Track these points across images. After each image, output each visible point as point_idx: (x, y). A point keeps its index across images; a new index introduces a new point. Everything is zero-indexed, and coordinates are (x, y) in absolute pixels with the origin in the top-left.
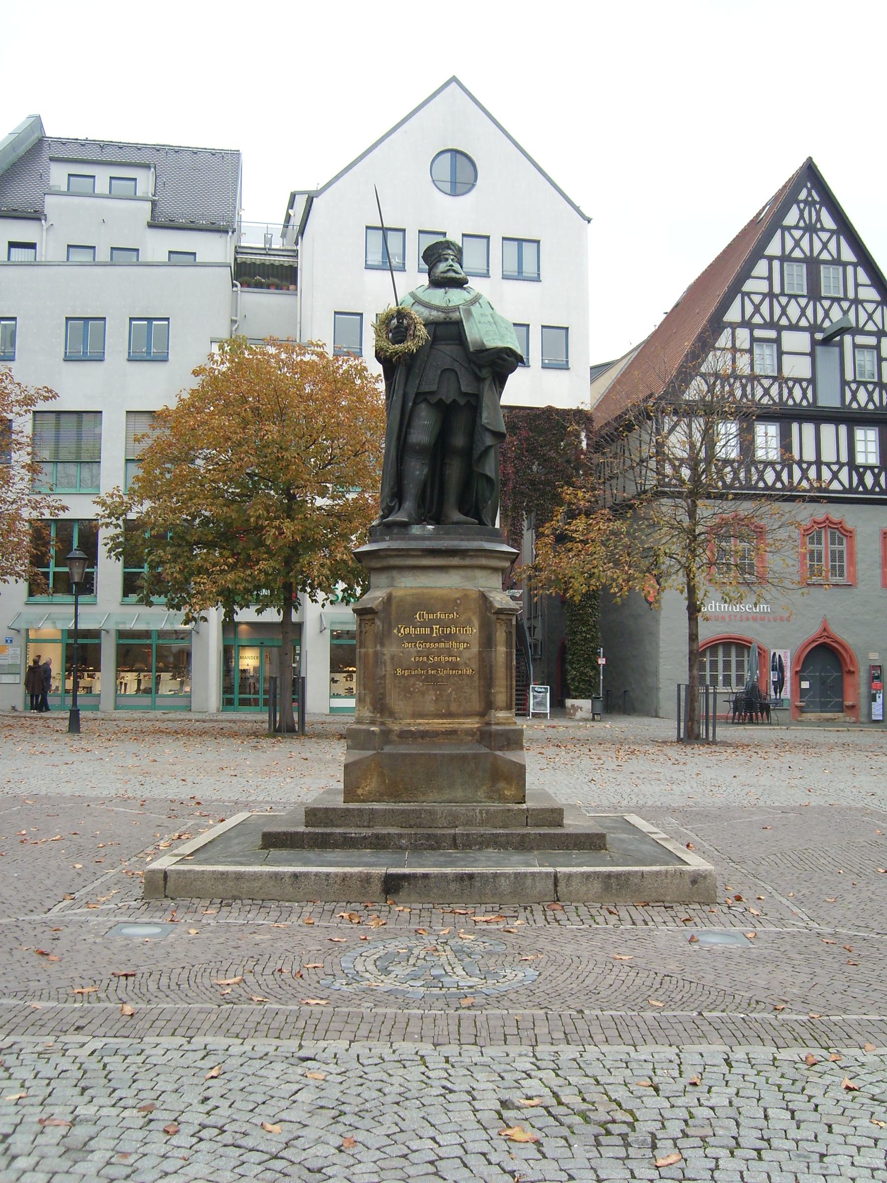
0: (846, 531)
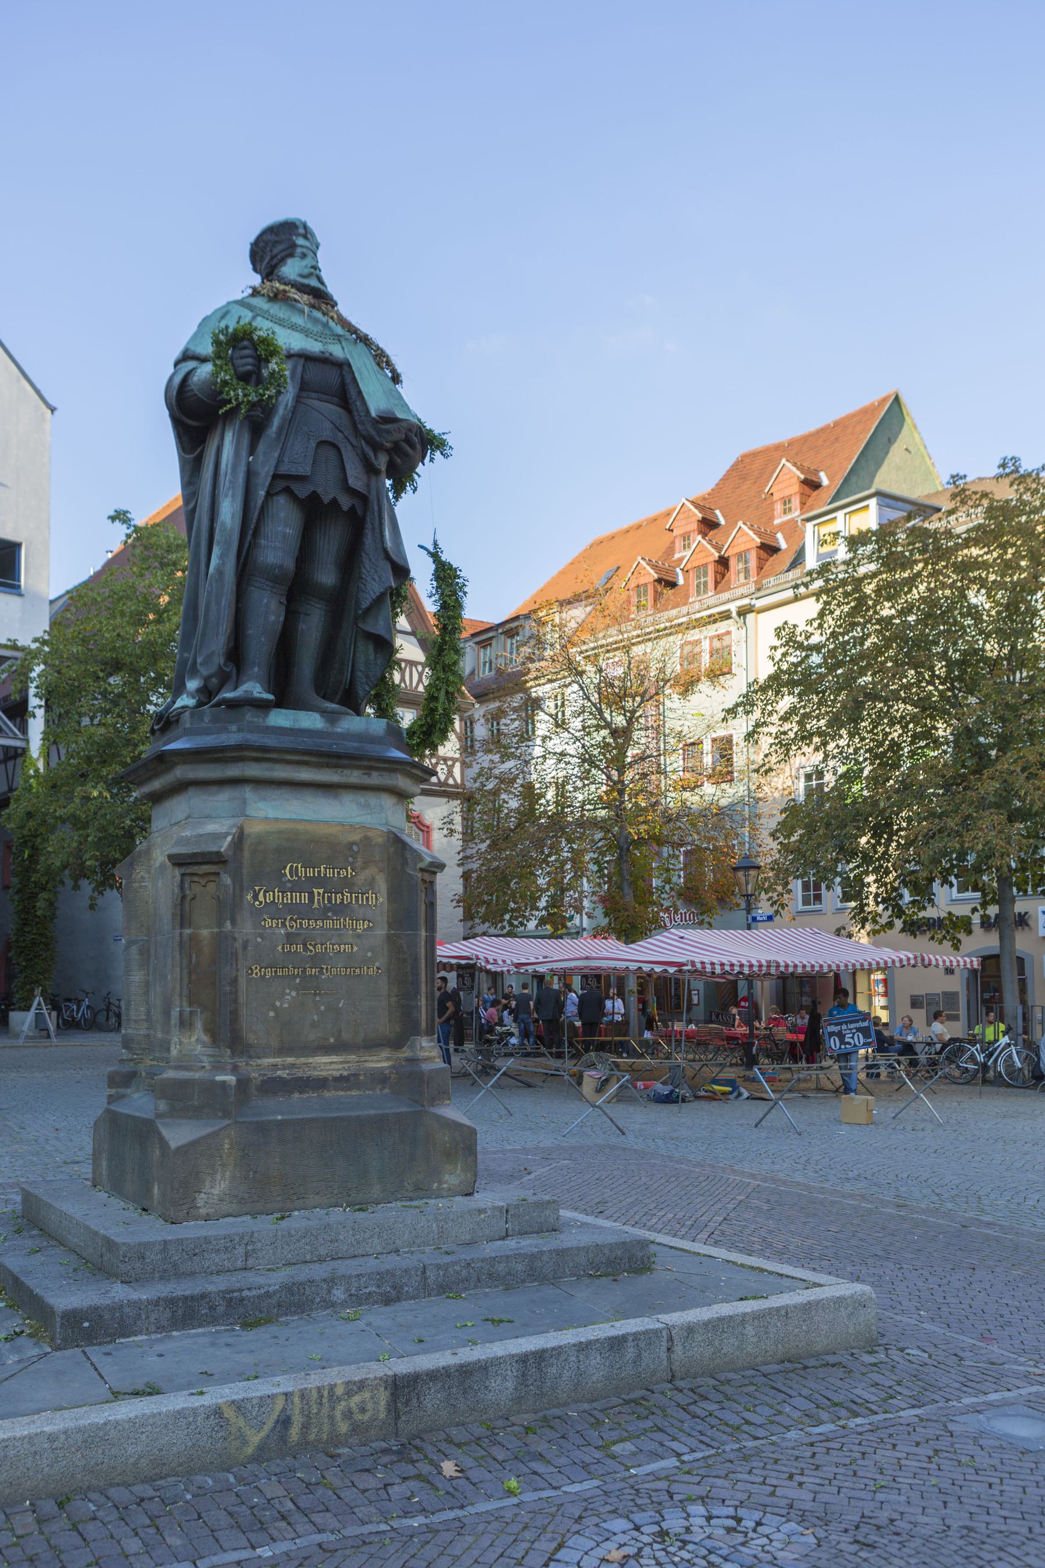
0: (424, 825)
